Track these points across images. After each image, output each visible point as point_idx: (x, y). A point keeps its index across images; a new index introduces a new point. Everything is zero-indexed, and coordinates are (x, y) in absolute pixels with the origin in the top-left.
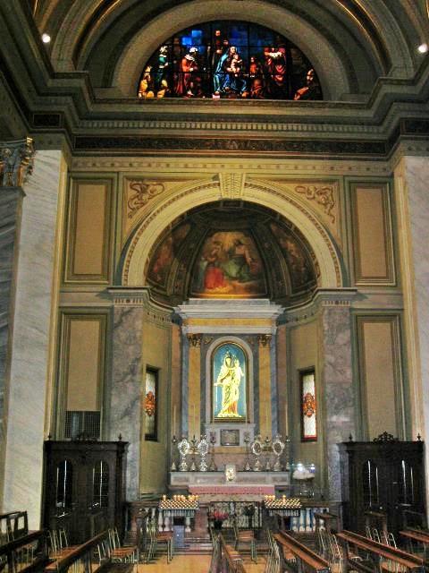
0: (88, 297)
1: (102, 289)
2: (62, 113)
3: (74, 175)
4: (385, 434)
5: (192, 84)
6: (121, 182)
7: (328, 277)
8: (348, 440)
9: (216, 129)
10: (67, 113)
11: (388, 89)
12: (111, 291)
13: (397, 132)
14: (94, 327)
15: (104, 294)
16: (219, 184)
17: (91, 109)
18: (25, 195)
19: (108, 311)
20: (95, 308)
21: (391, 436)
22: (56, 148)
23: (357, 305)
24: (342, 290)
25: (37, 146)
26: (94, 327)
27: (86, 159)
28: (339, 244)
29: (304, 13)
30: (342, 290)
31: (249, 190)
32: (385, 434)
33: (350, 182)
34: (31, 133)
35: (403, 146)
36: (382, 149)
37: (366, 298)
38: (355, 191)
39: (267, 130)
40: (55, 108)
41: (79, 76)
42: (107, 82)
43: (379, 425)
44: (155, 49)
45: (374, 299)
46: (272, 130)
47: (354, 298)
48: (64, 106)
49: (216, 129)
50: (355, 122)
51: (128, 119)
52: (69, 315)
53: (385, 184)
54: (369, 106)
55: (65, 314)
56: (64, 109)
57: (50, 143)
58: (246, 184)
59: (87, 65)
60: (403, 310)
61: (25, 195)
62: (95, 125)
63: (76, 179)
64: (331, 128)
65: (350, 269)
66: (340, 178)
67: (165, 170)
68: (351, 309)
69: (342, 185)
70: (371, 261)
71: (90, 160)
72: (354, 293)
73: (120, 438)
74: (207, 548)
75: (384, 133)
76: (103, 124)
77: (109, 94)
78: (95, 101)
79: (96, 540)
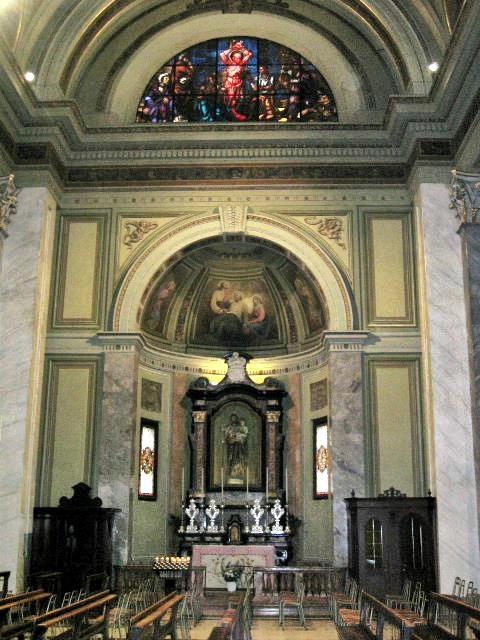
0: (77, 344)
1: (92, 334)
2: (49, 143)
3: (64, 212)
4: (392, 489)
5: (218, 110)
6: (114, 218)
7: (338, 318)
8: (350, 496)
9: (172, 157)
10: (55, 145)
11: (400, 109)
12: (101, 337)
13: (414, 157)
14: (84, 374)
15: (93, 341)
16: (219, 218)
17: (83, 140)
18: (6, 236)
19: (99, 358)
20: (62, 355)
21: (398, 492)
22: (43, 186)
23: (369, 349)
24: (352, 333)
25: (18, 185)
26: (84, 374)
27: (182, 193)
28: (351, 279)
29: (166, 21)
30: (352, 333)
31: (250, 223)
32: (392, 489)
33: (364, 213)
34: (13, 170)
35: (420, 171)
36: (397, 174)
37: (379, 340)
38: (370, 224)
39: (188, 157)
40: (44, 140)
41: (64, 103)
42: (101, 104)
43: (395, 479)
44: (150, 77)
45: (389, 342)
46: (118, 158)
47: (365, 342)
48: (53, 137)
49: (172, 157)
50: (364, 145)
51: (118, 149)
52: (54, 362)
53: (406, 214)
54: (384, 126)
55: (54, 361)
56: (51, 140)
57: (33, 180)
58: (248, 218)
59: (76, 94)
60: (420, 353)
61: (6, 236)
62: (99, 156)
63: (66, 218)
64: (334, 153)
65: (362, 307)
66: (355, 210)
67: (93, 206)
68: (363, 354)
69: (355, 216)
70: (388, 301)
71: (129, 195)
72: (365, 336)
73: (353, 494)
74: (272, 613)
75: (402, 156)
76: (113, 154)
77: (101, 120)
78: (88, 131)
79: (372, 601)
